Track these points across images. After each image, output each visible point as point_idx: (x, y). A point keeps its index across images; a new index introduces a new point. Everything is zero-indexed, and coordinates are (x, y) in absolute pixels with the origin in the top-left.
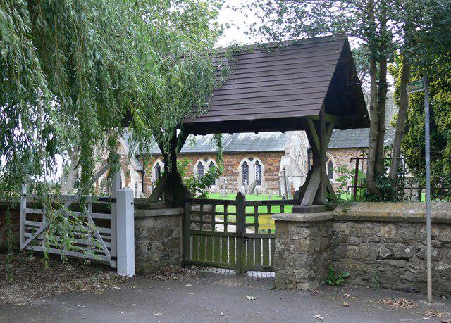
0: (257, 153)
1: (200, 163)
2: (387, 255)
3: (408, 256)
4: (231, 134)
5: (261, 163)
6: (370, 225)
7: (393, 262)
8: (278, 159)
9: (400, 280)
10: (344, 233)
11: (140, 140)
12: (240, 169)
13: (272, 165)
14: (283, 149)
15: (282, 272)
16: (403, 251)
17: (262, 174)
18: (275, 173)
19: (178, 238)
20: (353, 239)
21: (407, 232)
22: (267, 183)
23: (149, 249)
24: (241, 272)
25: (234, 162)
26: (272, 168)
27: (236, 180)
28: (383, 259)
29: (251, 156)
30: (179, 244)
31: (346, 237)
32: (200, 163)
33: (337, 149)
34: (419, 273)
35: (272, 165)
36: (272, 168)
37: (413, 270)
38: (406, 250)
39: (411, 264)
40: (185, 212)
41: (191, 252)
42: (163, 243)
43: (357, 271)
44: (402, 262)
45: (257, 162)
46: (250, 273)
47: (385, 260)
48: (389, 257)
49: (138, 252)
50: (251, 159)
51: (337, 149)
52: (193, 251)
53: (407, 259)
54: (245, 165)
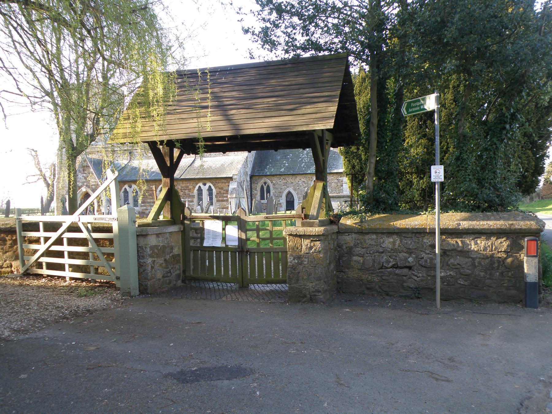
0: (210, 179)
1: (200, 187)
2: (391, 264)
3: (411, 265)
4: (250, 152)
5: (213, 187)
6: (374, 236)
7: (398, 271)
8: (227, 184)
9: (403, 287)
10: (348, 245)
11: (548, 52)
12: (196, 192)
13: (222, 188)
14: (231, 176)
15: (295, 285)
16: (406, 259)
17: (214, 196)
18: (225, 195)
19: (179, 255)
20: (358, 250)
21: (410, 243)
22: (218, 204)
23: (152, 267)
24: (243, 286)
25: (191, 187)
26: (222, 191)
27: (193, 201)
28: (387, 268)
29: (205, 181)
30: (179, 260)
31: (351, 248)
32: (200, 187)
33: (274, 175)
34: (422, 280)
35: (222, 188)
36: (222, 191)
37: (416, 278)
38: (409, 259)
39: (414, 273)
40: (184, 228)
41: (192, 267)
42: (165, 260)
43: (362, 280)
44: (406, 271)
45: (210, 187)
46: (252, 287)
47: (389, 270)
48: (395, 266)
49: (142, 270)
50: (205, 184)
51: (274, 175)
52: (194, 265)
53: (410, 268)
54: (200, 189)
